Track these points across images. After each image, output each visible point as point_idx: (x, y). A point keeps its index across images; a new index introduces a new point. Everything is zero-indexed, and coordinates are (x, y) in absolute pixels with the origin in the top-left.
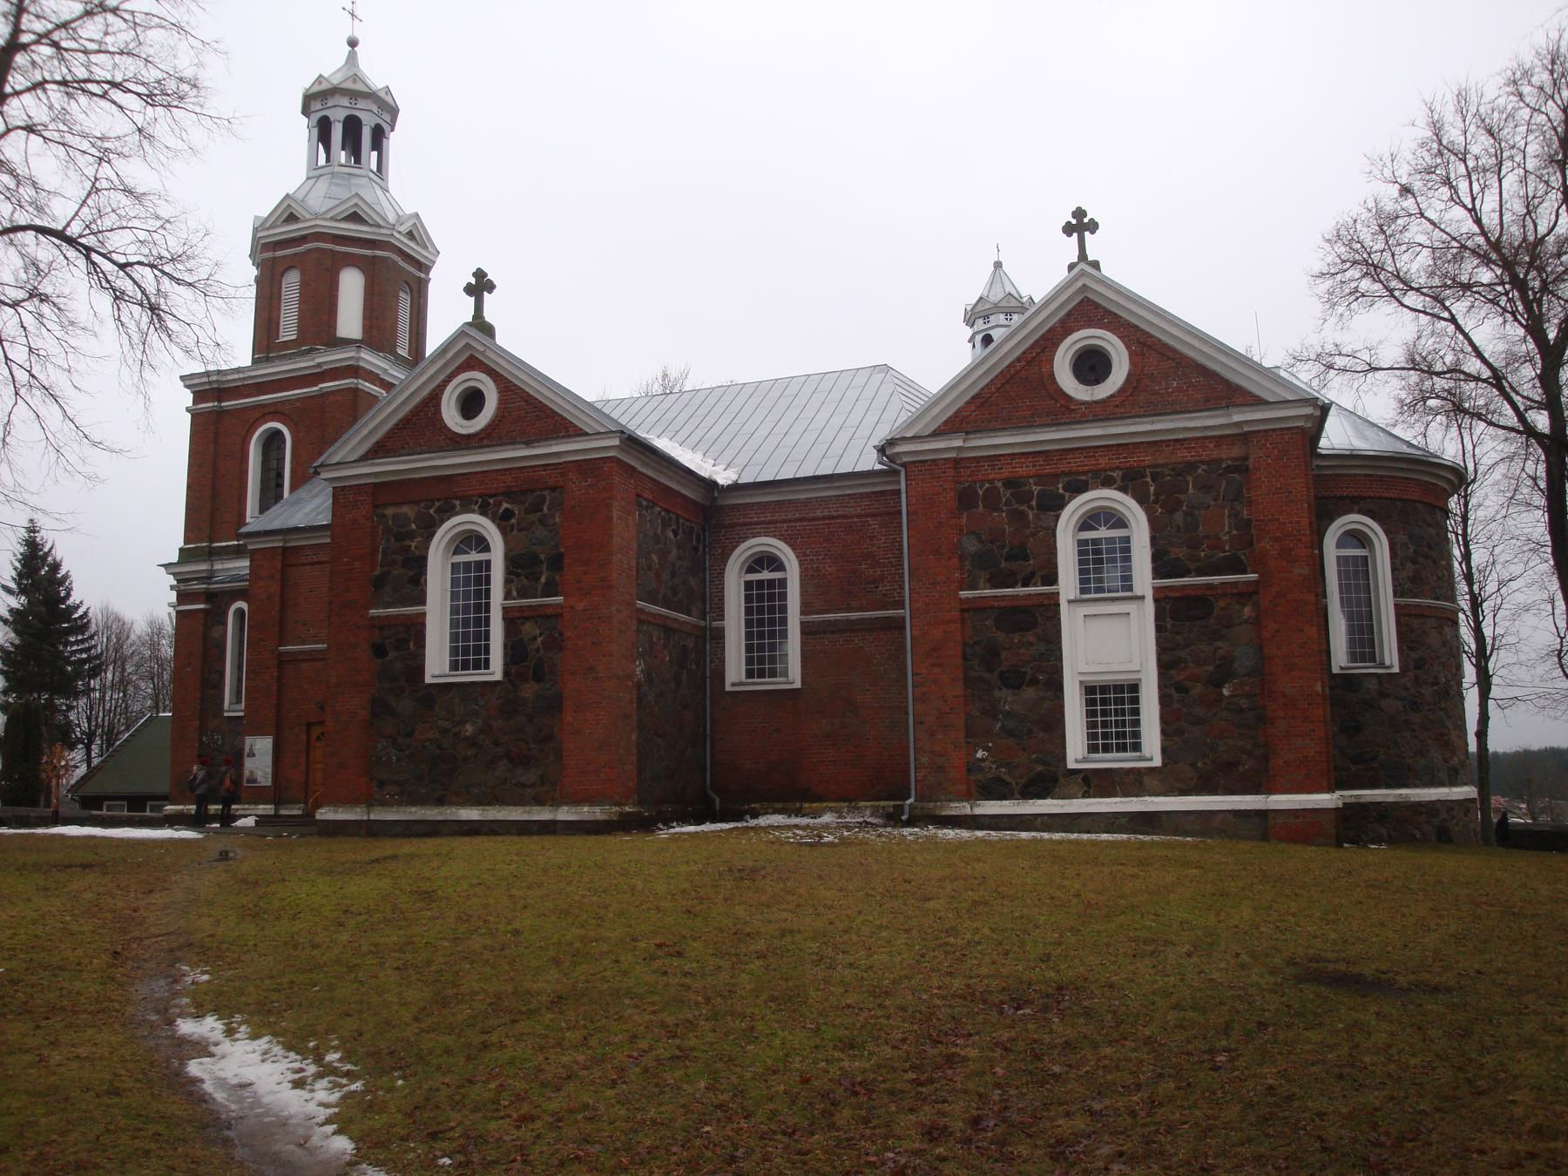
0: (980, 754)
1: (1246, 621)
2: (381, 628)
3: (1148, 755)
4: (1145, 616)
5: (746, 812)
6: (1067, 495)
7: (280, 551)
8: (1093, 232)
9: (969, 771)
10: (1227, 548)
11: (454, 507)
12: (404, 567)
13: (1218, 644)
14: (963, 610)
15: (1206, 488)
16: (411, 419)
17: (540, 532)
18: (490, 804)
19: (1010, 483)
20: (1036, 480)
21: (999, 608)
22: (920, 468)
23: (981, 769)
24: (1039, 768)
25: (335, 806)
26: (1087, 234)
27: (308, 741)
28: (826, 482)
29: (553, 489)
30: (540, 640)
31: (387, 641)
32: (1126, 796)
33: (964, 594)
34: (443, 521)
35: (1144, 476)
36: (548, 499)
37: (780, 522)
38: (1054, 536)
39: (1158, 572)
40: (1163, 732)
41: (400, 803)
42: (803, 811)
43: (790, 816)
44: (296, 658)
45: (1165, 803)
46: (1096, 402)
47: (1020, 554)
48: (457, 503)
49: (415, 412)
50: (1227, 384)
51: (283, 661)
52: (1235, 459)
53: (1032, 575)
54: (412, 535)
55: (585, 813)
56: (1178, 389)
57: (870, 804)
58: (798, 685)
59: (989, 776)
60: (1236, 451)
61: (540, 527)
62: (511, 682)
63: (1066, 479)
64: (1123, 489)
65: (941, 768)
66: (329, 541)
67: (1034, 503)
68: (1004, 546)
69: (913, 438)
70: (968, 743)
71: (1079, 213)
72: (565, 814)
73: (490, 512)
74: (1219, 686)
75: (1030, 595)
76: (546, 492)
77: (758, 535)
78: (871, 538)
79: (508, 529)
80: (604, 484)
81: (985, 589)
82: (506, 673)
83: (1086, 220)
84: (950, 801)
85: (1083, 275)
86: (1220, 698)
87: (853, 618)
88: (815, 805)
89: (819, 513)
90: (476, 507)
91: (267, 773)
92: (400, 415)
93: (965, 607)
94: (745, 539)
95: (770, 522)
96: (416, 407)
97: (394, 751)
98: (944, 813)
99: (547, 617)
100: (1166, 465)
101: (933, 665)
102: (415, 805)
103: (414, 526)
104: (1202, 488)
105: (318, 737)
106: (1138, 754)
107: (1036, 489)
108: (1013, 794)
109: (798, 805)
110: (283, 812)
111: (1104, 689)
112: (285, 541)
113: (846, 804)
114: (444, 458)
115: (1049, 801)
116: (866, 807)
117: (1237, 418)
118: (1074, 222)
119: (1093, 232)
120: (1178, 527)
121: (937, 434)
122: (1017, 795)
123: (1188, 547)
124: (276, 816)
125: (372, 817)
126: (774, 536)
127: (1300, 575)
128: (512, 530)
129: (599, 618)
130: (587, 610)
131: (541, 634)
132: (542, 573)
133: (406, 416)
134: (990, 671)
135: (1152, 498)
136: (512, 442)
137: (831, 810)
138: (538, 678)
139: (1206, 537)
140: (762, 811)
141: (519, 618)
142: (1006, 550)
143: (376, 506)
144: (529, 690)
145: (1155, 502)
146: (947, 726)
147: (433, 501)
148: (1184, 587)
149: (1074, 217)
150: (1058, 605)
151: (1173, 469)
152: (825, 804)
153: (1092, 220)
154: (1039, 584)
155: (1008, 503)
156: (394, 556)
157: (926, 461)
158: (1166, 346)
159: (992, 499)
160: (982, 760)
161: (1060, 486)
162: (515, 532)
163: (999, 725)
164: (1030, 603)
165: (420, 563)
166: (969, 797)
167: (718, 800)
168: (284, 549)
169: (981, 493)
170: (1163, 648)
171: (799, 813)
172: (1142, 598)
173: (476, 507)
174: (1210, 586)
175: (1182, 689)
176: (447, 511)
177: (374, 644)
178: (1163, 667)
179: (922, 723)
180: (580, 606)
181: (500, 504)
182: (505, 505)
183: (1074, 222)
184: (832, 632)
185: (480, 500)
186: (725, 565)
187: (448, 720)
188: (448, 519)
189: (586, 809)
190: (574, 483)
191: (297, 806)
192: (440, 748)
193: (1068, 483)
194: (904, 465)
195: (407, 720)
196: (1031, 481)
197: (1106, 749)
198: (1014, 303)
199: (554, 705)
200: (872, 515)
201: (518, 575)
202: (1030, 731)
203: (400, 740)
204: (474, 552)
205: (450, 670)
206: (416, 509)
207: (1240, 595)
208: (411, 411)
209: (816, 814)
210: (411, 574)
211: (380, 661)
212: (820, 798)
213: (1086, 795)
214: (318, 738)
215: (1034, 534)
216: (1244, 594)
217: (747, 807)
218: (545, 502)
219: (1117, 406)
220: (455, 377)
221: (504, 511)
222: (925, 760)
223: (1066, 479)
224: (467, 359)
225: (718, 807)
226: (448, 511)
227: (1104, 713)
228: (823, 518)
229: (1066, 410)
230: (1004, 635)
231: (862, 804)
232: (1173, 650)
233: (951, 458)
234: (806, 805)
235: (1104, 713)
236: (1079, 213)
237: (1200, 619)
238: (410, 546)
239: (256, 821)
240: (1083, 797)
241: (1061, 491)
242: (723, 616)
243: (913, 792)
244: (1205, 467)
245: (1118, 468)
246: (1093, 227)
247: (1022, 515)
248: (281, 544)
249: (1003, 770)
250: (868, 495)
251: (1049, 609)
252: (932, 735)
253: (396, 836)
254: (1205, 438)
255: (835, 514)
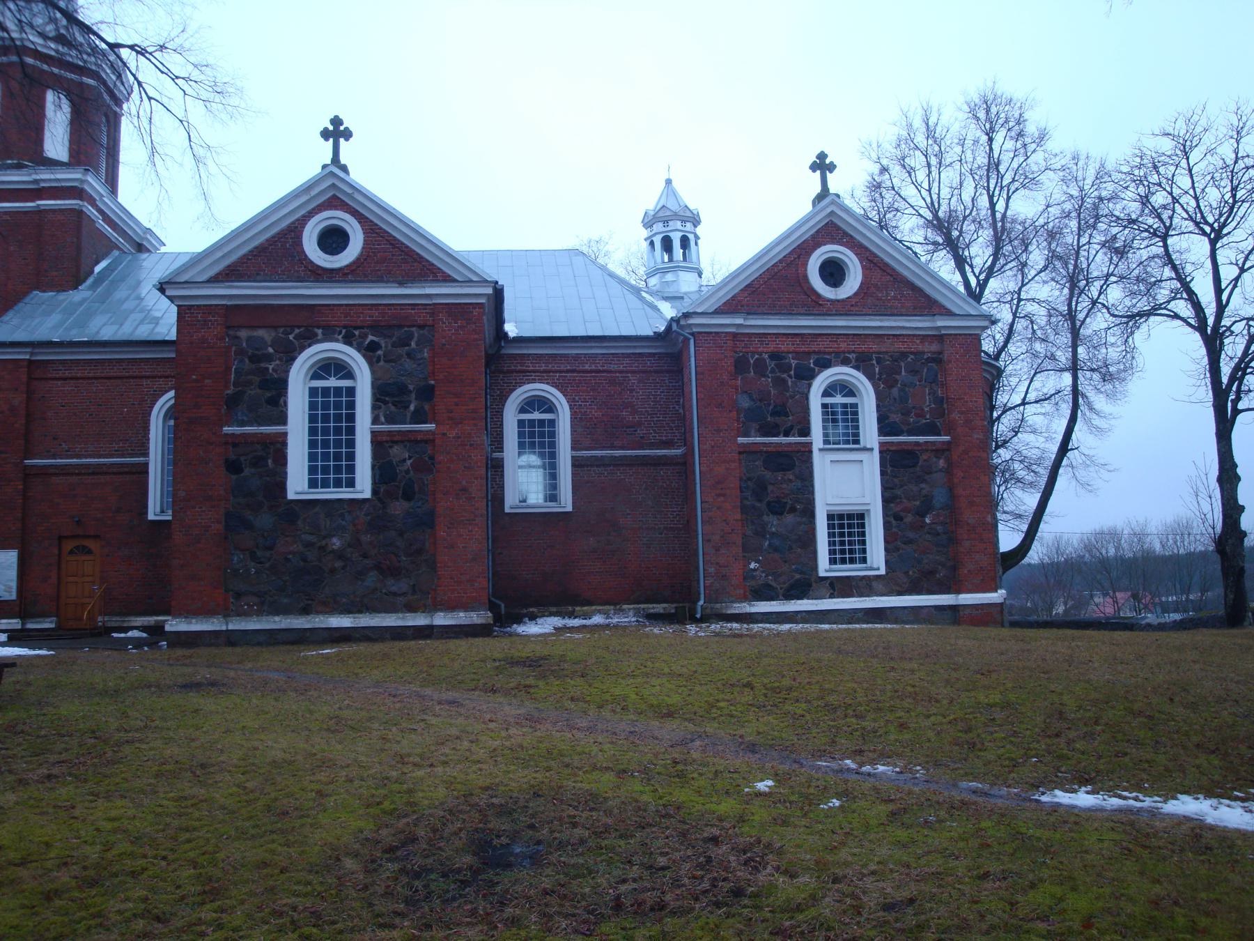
0: (753, 565)
1: (940, 470)
2: (235, 445)
3: (875, 566)
4: (872, 464)
5: (525, 615)
6: (817, 369)
7: (25, 363)
8: (347, 140)
9: (745, 578)
10: (928, 417)
11: (316, 335)
12: (260, 388)
13: (923, 485)
14: (740, 453)
15: (913, 371)
16: (267, 248)
17: (409, 365)
18: (360, 612)
19: (775, 356)
20: (794, 355)
21: (766, 452)
22: (706, 337)
23: (753, 578)
24: (798, 576)
25: (186, 617)
26: (342, 140)
27: (60, 556)
28: (596, 342)
29: (421, 327)
30: (409, 462)
31: (242, 459)
32: (861, 596)
33: (741, 440)
34: (303, 348)
35: (871, 359)
36: (416, 335)
37: (553, 372)
38: (807, 399)
39: (883, 431)
40: (886, 549)
41: (259, 613)
42: (576, 614)
43: (564, 618)
44: (44, 472)
45: (889, 601)
46: (838, 301)
47: (781, 411)
48: (319, 331)
49: (272, 241)
50: (928, 297)
51: (29, 475)
52: (934, 353)
53: (792, 428)
54: (269, 358)
55: (461, 618)
56: (895, 298)
57: (632, 606)
58: (569, 508)
59: (760, 582)
60: (934, 347)
61: (408, 360)
62: (380, 500)
63: (816, 357)
64: (857, 368)
65: (724, 577)
66: (174, 356)
67: (792, 373)
68: (769, 405)
69: (702, 313)
70: (744, 556)
71: (336, 121)
72: (441, 619)
73: (354, 343)
74: (923, 516)
75: (790, 443)
76: (414, 329)
77: (534, 381)
78: (631, 391)
79: (375, 360)
80: (474, 327)
81: (756, 437)
82: (375, 492)
83: (342, 128)
84: (732, 602)
85: (832, 203)
86: (923, 525)
87: (617, 455)
88: (585, 608)
89: (587, 367)
90: (340, 337)
91: (10, 588)
92: (256, 243)
93: (742, 450)
94: (521, 384)
95: (545, 371)
96: (273, 237)
97: (253, 564)
98: (729, 612)
99: (417, 442)
100: (887, 353)
101: (719, 495)
102: (278, 615)
103: (271, 350)
104: (911, 371)
105: (71, 550)
106: (865, 565)
107: (794, 363)
108: (778, 596)
109: (570, 608)
110: (30, 626)
111: (841, 517)
112: (32, 354)
113: (612, 607)
114: (310, 288)
115: (805, 601)
116: (629, 609)
117: (940, 324)
118: (331, 128)
119: (347, 140)
120: (895, 399)
121: (717, 312)
122: (781, 597)
123: (902, 414)
124: (23, 630)
125: (231, 627)
126: (548, 383)
127: (977, 439)
128: (378, 360)
129: (471, 445)
130: (459, 437)
131: (410, 458)
132: (410, 402)
133: (262, 244)
134: (760, 501)
135: (877, 376)
136: (379, 279)
137: (600, 612)
138: (408, 496)
139: (914, 408)
140: (539, 615)
141: (387, 442)
142: (771, 407)
143: (228, 327)
144: (398, 508)
145: (879, 379)
146: (729, 543)
147: (293, 327)
148: (899, 443)
149: (332, 124)
150: (811, 452)
151: (891, 356)
152: (594, 607)
153: (346, 129)
154: (796, 435)
155: (773, 371)
156: (249, 377)
157: (711, 333)
158: (887, 265)
159: (760, 367)
160: (755, 570)
161: (812, 361)
162: (382, 363)
163: (767, 544)
164: (790, 449)
165: (281, 386)
166: (744, 598)
167: (503, 605)
168: (29, 361)
169: (752, 362)
170: (885, 488)
171: (572, 615)
172: (872, 449)
173: (340, 337)
174: (917, 444)
175: (898, 518)
176: (309, 339)
177: (227, 461)
178: (886, 501)
179: (709, 541)
180: (452, 434)
181: (366, 336)
182: (371, 338)
183: (331, 128)
184: (598, 466)
185: (344, 331)
186: (504, 405)
187: (312, 534)
188: (310, 346)
189: (462, 614)
190: (444, 323)
191: (49, 620)
192: (304, 560)
193: (817, 359)
194: (693, 334)
195: (266, 534)
196: (790, 356)
197: (843, 561)
198: (689, 214)
199: (427, 521)
200: (633, 372)
201: (385, 403)
202: (791, 548)
203: (259, 553)
204: (333, 378)
205: (309, 487)
206: (273, 334)
207: (937, 451)
208: (267, 240)
209: (587, 616)
210: (268, 394)
211: (234, 477)
212: (589, 603)
213: (832, 596)
214: (71, 552)
215: (792, 397)
216: (940, 450)
217: (525, 611)
218: (413, 338)
219: (852, 306)
220: (317, 213)
221: (369, 343)
222: (712, 570)
223: (816, 357)
224: (329, 199)
225: (503, 612)
226: (309, 339)
227: (850, 534)
228: (591, 372)
229: (816, 305)
230: (770, 473)
231: (625, 607)
232: (893, 489)
233: (730, 333)
234: (578, 608)
235: (850, 534)
236: (336, 121)
237: (911, 467)
238: (267, 369)
239: (8, 637)
240: (830, 597)
241: (812, 365)
242: (502, 448)
243: (702, 596)
244: (912, 357)
245: (853, 352)
246: (347, 135)
247: (784, 381)
248: (28, 357)
249: (770, 577)
250: (628, 355)
251: (805, 453)
252: (718, 550)
253: (259, 644)
254: (914, 335)
255: (601, 368)
